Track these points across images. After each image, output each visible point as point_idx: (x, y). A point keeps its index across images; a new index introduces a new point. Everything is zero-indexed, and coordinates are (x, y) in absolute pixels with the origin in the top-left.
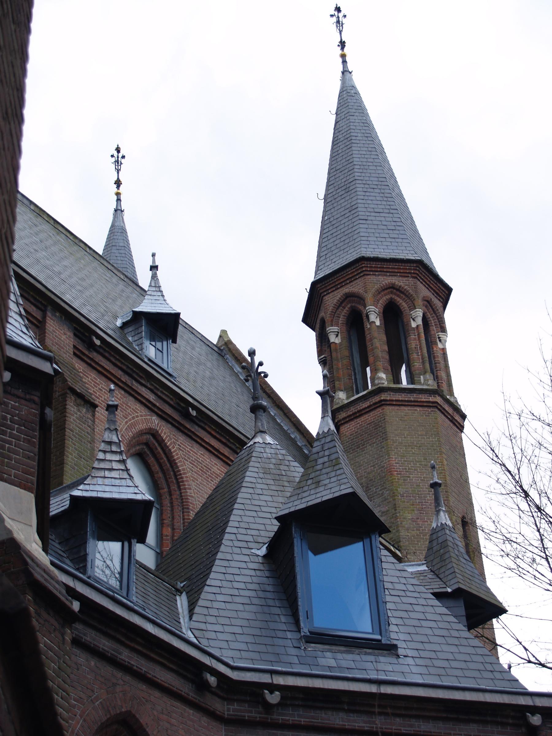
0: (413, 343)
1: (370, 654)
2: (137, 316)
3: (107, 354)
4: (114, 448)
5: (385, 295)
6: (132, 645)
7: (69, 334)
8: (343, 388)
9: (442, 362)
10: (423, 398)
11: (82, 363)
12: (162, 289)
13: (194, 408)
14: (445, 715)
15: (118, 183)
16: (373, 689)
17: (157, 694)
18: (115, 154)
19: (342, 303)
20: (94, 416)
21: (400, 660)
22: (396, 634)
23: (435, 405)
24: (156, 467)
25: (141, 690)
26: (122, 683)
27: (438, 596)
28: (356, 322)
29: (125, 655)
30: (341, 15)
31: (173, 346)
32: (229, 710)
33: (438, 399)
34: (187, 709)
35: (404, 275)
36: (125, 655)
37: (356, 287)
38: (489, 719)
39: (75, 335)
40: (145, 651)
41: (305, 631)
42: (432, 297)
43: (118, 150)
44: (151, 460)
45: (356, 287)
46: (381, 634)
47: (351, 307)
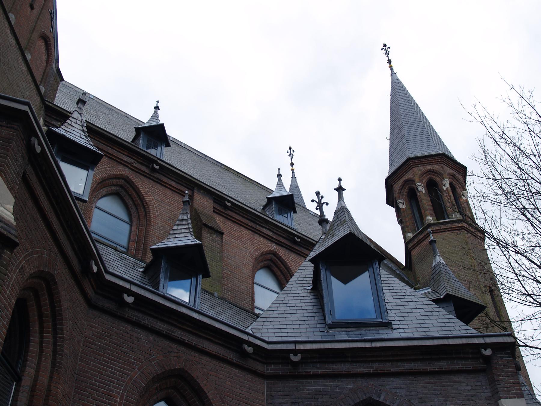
0: (446, 198)
1: (373, 330)
2: (270, 200)
3: (237, 212)
4: (184, 222)
5: (426, 176)
6: (184, 327)
7: (210, 201)
8: (410, 231)
9: (466, 206)
10: (455, 225)
11: (221, 217)
12: (284, 185)
13: (298, 237)
14: (421, 357)
15: (292, 165)
16: (368, 345)
17: (207, 359)
18: (289, 151)
19: (403, 186)
20: (222, 239)
21: (394, 331)
22: (391, 317)
23: (463, 228)
24: (279, 273)
25: (194, 356)
26: (177, 351)
27: (436, 301)
28: (412, 195)
29: (178, 334)
30: (386, 47)
31: (294, 215)
32: (268, 370)
33: (464, 225)
34: (234, 369)
35: (435, 163)
36: (178, 334)
37: (409, 176)
38: (454, 356)
39: (214, 202)
40: (194, 331)
41: (329, 322)
42: (455, 173)
43: (290, 148)
44: (275, 269)
45: (409, 176)
46: (382, 319)
47: (409, 187)
